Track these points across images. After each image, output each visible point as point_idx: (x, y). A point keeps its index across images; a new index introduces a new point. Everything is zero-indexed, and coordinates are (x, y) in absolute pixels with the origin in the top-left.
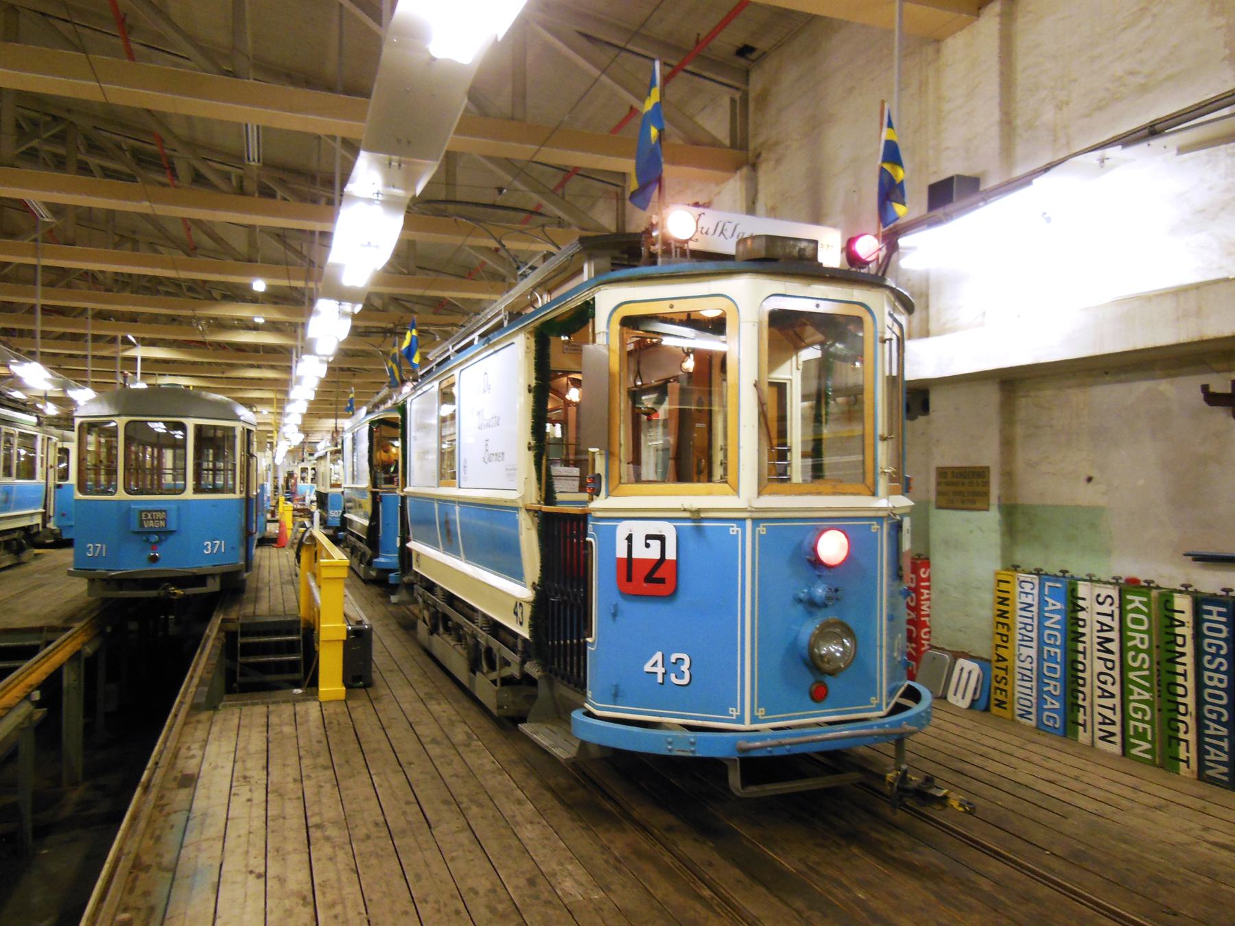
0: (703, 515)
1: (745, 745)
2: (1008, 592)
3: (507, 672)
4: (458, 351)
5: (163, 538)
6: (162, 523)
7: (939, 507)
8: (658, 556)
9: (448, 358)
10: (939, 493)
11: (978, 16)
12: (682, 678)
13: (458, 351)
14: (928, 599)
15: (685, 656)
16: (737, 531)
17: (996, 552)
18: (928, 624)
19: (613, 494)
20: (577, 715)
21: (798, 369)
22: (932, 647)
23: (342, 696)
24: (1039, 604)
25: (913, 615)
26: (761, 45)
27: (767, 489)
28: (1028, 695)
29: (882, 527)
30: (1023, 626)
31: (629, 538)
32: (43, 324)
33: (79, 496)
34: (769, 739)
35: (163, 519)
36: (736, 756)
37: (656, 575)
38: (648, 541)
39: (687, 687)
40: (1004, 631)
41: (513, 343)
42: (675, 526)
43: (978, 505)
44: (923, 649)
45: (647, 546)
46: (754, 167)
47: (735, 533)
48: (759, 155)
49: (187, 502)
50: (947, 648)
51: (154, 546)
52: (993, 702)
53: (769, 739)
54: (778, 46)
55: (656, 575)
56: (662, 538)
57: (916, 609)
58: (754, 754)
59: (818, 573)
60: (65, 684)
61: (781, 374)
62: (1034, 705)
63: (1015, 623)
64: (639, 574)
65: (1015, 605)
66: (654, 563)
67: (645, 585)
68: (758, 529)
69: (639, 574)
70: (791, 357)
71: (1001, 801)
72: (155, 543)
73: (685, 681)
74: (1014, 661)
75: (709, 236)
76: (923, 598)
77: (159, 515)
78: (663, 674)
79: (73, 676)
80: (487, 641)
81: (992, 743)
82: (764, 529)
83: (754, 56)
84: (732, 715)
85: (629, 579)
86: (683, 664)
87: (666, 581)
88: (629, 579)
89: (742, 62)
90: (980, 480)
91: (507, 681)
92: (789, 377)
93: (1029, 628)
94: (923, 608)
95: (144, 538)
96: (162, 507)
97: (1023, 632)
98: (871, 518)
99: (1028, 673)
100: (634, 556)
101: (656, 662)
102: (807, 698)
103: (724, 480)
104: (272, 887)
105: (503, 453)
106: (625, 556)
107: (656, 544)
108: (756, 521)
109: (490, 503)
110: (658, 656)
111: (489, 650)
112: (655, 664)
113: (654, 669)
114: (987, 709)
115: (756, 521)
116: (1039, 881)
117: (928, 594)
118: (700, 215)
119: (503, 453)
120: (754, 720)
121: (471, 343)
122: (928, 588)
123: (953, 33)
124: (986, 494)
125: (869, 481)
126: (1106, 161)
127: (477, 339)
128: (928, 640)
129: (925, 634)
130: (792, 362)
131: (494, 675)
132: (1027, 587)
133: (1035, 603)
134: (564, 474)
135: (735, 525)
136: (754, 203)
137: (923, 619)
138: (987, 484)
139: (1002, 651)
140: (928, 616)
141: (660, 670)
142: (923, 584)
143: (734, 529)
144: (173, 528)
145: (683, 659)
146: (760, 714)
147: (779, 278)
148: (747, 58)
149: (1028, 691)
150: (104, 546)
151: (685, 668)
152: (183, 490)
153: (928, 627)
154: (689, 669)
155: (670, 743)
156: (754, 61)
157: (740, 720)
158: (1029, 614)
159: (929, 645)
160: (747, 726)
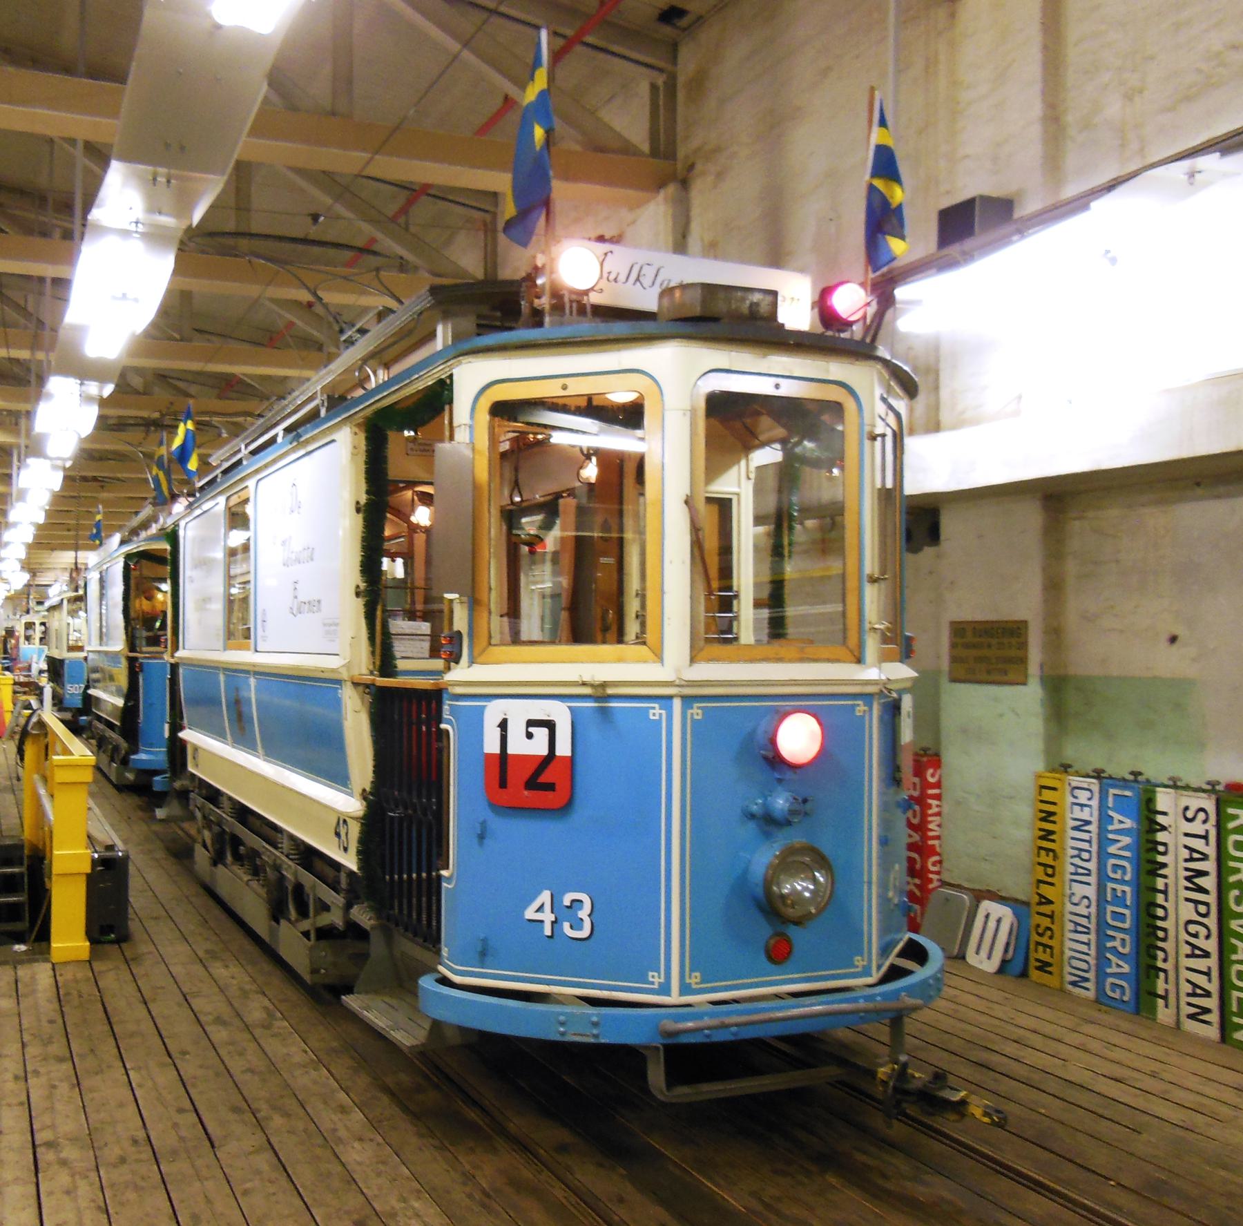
0: (610, 691)
2: (1054, 804)
3: (325, 920)
7: (954, 680)
8: (544, 751)
9: (239, 462)
10: (954, 659)
12: (580, 928)
16: (660, 714)
18: (938, 850)
21: (749, 478)
22: (944, 884)
25: (916, 837)
31: (503, 725)
41: (333, 441)
44: (931, 886)
45: (530, 736)
46: (685, 184)
47: (657, 717)
48: (691, 167)
50: (966, 885)
52: (1033, 963)
56: (550, 725)
57: (920, 828)
58: (684, 1039)
64: (517, 777)
65: (1064, 823)
66: (540, 760)
67: (526, 793)
69: (517, 777)
70: (738, 462)
74: (1063, 904)
76: (930, 812)
78: (553, 923)
80: (295, 874)
83: (684, 22)
85: (503, 784)
86: (581, 909)
88: (503, 784)
89: (667, 30)
90: (1014, 641)
91: (325, 934)
92: (736, 490)
93: (1085, 855)
94: (931, 826)
97: (1077, 861)
102: (763, 958)
103: (641, 640)
107: (541, 734)
108: (688, 700)
110: (545, 897)
112: (540, 909)
113: (538, 916)
114: (1024, 974)
115: (688, 700)
118: (606, 254)
120: (685, 989)
121: (273, 441)
122: (938, 797)
124: (1023, 661)
125: (853, 640)
128: (938, 873)
129: (934, 864)
131: (306, 925)
132: (1083, 797)
135: (656, 705)
136: (684, 236)
137: (931, 842)
138: (1023, 646)
139: (1046, 890)
140: (938, 838)
141: (548, 917)
142: (931, 792)
143: (861, 708)
148: (674, 25)
149: (1084, 948)
151: (584, 913)
153: (939, 854)
154: (589, 916)
155: (562, 1024)
156: (684, 30)
157: (665, 989)
158: (1085, 836)
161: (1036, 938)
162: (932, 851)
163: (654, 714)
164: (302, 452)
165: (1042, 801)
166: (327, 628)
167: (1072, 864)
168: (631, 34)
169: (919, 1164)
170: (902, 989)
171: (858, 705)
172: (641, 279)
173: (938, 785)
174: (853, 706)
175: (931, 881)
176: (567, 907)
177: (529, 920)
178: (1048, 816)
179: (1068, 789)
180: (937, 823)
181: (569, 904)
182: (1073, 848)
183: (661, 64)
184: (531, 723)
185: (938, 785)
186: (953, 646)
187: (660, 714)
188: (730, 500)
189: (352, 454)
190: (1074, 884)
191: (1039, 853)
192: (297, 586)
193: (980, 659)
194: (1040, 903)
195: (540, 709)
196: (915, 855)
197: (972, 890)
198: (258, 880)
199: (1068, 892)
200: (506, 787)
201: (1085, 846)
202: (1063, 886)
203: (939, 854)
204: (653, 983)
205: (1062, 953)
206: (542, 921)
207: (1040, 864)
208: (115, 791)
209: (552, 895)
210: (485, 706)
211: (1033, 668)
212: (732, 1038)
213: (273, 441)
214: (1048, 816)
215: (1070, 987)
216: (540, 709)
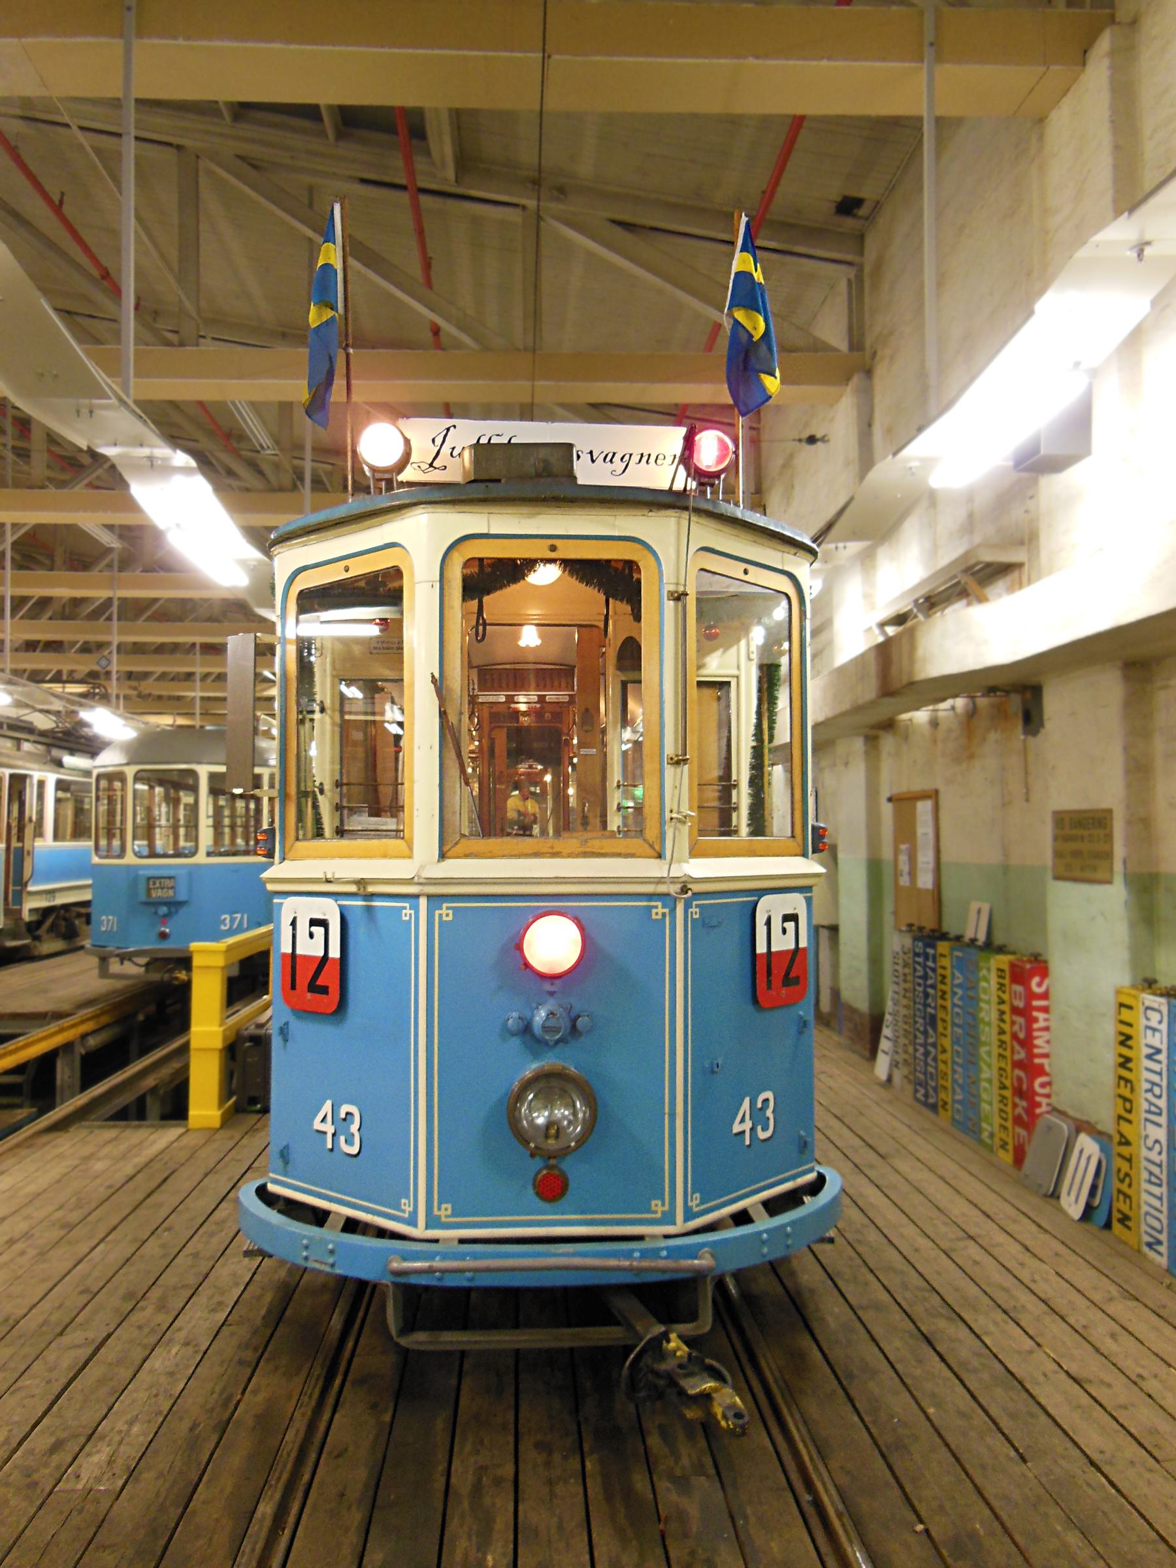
0: (371, 889)
2: (1130, 1025)
5: (173, 910)
6: (171, 892)
7: (1057, 878)
8: (321, 953)
10: (1058, 854)
11: (1084, 64)
14: (1047, 1029)
15: (354, 1109)
17: (1121, 954)
18: (1047, 1068)
21: (750, 659)
22: (1055, 1110)
23: (217, 1123)
24: (1168, 1048)
25: (1021, 1055)
26: (868, 192)
27: (459, 849)
28: (1156, 1209)
29: (673, 910)
30: (1148, 1086)
32: (11, 663)
33: (96, 860)
35: (172, 888)
39: (354, 1159)
40: (1126, 1092)
42: (340, 906)
43: (1099, 875)
44: (1038, 1111)
46: (869, 372)
48: (875, 354)
49: (198, 866)
50: (1071, 1112)
51: (165, 919)
52: (1116, 1215)
53: (438, 1258)
54: (891, 188)
57: (1027, 1043)
58: (414, 1280)
60: (59, 1082)
61: (716, 666)
62: (1165, 1230)
63: (1139, 1081)
64: (778, 972)
65: (1139, 1049)
67: (309, 995)
68: (437, 912)
71: (938, 1406)
72: (165, 916)
73: (354, 1150)
74: (1139, 1146)
76: (1035, 1026)
77: (168, 883)
78: (334, 1135)
79: (67, 1073)
81: (1050, 1287)
83: (863, 211)
84: (439, 1209)
85: (293, 987)
87: (330, 990)
88: (293, 987)
89: (849, 223)
90: (1102, 832)
92: (735, 672)
93: (1157, 1090)
94: (1037, 1042)
95: (153, 910)
96: (171, 873)
97: (1149, 1096)
98: (650, 896)
99: (1156, 1170)
100: (299, 951)
104: (905, 1299)
106: (290, 951)
108: (435, 900)
113: (322, 1127)
114: (1108, 1225)
117: (1046, 1020)
118: (448, 429)
120: (432, 1222)
122: (1045, 1010)
123: (1056, 102)
124: (1109, 856)
125: (651, 833)
126: (1148, 251)
128: (1048, 1096)
129: (1043, 1085)
130: (738, 650)
132: (1154, 1017)
133: (1164, 1047)
134: (372, 827)
135: (407, 905)
136: (870, 425)
137: (1037, 1061)
138: (1109, 837)
139: (1125, 1128)
140: (1046, 1056)
141: (329, 1128)
142: (1036, 1003)
143: (659, 910)
144: (182, 896)
146: (443, 1213)
147: (593, 512)
148: (855, 216)
149: (1156, 1203)
150: (245, 916)
152: (194, 853)
153: (1047, 1074)
155: (306, 1247)
156: (867, 219)
157: (413, 1222)
158: (1156, 1067)
159: (1048, 1105)
160: (419, 1231)
161: (1116, 1184)
162: (1040, 1071)
163: (447, 915)
165: (1122, 1022)
167: (1146, 1100)
168: (815, 233)
169: (708, 1461)
170: (704, 1245)
171: (405, 908)
173: (1045, 996)
174: (650, 908)
175: (1039, 1105)
177: (318, 1131)
178: (1125, 1040)
179: (1142, 1009)
180: (1045, 1039)
182: (1147, 1081)
183: (849, 258)
185: (1045, 996)
186: (1056, 838)
190: (1148, 1124)
191: (1119, 1085)
193: (1077, 854)
194: (1120, 1143)
196: (1022, 1074)
197: (1075, 1120)
199: (1143, 1133)
201: (1156, 1079)
202: (1139, 1124)
203: (1047, 1074)
205: (1139, 1207)
206: (325, 1133)
207: (1120, 1096)
211: (1118, 866)
212: (466, 1284)
214: (1125, 1040)
215: (1146, 1249)
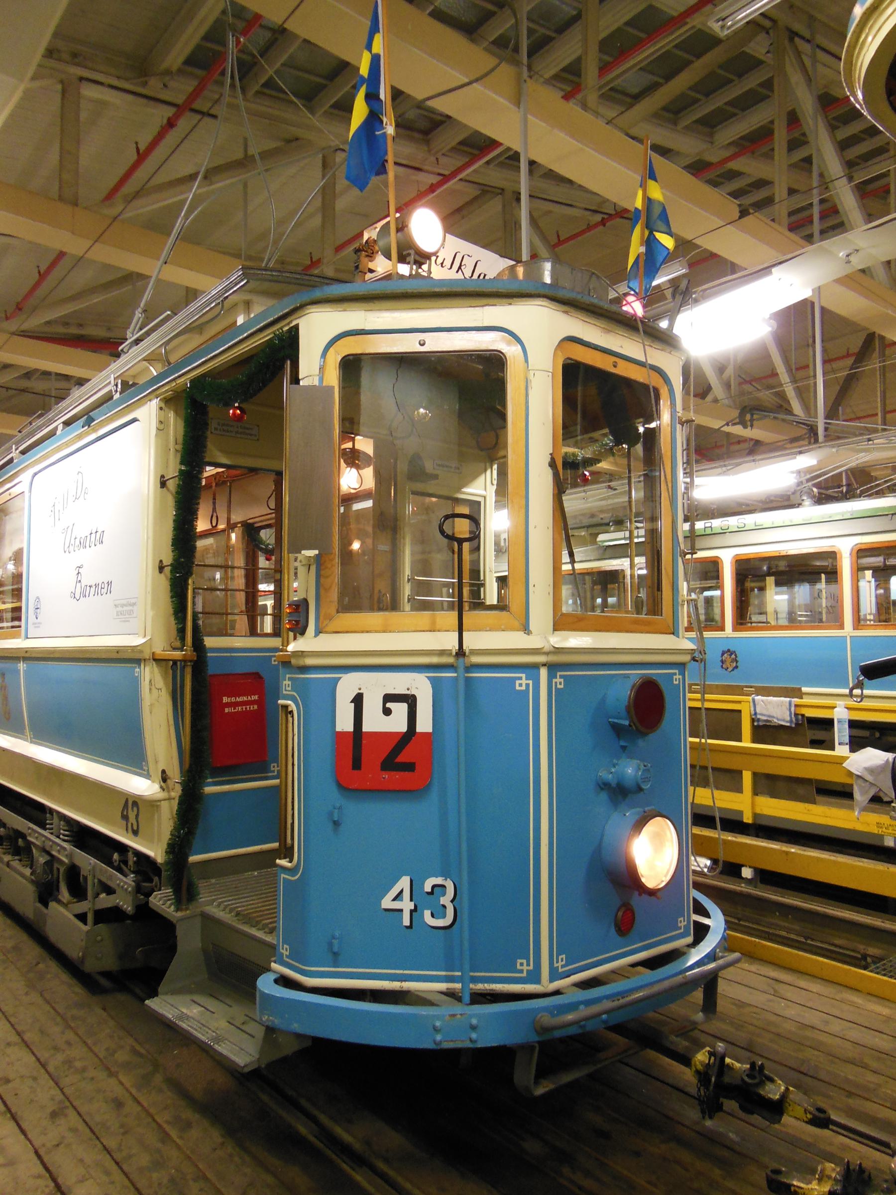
1: (547, 1020)
3: (105, 901)
4: (23, 452)
8: (403, 728)
9: (11, 461)
12: (444, 916)
13: (23, 452)
16: (528, 685)
19: (330, 628)
20: (266, 984)
31: (358, 701)
34: (582, 1007)
36: (534, 1038)
37: (400, 759)
38: (388, 705)
41: (134, 420)
45: (387, 712)
47: (524, 688)
55: (400, 759)
56: (410, 700)
59: (622, 743)
64: (372, 758)
66: (401, 735)
68: (554, 680)
69: (372, 758)
70: (485, 471)
73: (447, 921)
75: (445, 268)
78: (411, 911)
80: (70, 856)
82: (562, 680)
85: (357, 764)
86: (444, 894)
88: (357, 764)
91: (104, 916)
92: (483, 492)
101: (402, 891)
102: (613, 931)
103: (502, 606)
105: (109, 584)
107: (400, 710)
108: (553, 668)
109: (87, 656)
110: (404, 883)
111: (73, 873)
112: (398, 897)
113: (397, 905)
115: (553, 668)
116: (840, 1134)
119: (109, 584)
120: (555, 975)
121: (53, 433)
127: (61, 427)
131: (83, 906)
135: (523, 676)
141: (406, 905)
143: (522, 682)
145: (444, 886)
151: (446, 900)
154: (452, 901)
157: (535, 977)
164: (93, 436)
166: (120, 609)
172: (462, 268)
176: (428, 893)
181: (429, 890)
184: (388, 698)
187: (528, 685)
188: (479, 503)
189: (158, 429)
192: (81, 570)
195: (399, 683)
198: (20, 860)
200: (360, 769)
204: (521, 971)
206: (401, 910)
208: (78, 991)
209: (411, 881)
210: (340, 678)
213: (53, 433)
216: (399, 683)
